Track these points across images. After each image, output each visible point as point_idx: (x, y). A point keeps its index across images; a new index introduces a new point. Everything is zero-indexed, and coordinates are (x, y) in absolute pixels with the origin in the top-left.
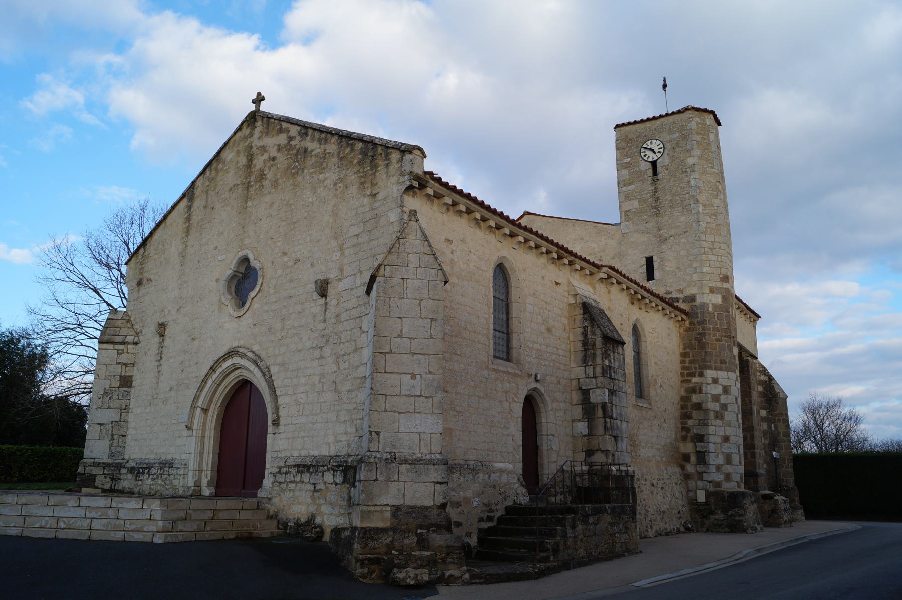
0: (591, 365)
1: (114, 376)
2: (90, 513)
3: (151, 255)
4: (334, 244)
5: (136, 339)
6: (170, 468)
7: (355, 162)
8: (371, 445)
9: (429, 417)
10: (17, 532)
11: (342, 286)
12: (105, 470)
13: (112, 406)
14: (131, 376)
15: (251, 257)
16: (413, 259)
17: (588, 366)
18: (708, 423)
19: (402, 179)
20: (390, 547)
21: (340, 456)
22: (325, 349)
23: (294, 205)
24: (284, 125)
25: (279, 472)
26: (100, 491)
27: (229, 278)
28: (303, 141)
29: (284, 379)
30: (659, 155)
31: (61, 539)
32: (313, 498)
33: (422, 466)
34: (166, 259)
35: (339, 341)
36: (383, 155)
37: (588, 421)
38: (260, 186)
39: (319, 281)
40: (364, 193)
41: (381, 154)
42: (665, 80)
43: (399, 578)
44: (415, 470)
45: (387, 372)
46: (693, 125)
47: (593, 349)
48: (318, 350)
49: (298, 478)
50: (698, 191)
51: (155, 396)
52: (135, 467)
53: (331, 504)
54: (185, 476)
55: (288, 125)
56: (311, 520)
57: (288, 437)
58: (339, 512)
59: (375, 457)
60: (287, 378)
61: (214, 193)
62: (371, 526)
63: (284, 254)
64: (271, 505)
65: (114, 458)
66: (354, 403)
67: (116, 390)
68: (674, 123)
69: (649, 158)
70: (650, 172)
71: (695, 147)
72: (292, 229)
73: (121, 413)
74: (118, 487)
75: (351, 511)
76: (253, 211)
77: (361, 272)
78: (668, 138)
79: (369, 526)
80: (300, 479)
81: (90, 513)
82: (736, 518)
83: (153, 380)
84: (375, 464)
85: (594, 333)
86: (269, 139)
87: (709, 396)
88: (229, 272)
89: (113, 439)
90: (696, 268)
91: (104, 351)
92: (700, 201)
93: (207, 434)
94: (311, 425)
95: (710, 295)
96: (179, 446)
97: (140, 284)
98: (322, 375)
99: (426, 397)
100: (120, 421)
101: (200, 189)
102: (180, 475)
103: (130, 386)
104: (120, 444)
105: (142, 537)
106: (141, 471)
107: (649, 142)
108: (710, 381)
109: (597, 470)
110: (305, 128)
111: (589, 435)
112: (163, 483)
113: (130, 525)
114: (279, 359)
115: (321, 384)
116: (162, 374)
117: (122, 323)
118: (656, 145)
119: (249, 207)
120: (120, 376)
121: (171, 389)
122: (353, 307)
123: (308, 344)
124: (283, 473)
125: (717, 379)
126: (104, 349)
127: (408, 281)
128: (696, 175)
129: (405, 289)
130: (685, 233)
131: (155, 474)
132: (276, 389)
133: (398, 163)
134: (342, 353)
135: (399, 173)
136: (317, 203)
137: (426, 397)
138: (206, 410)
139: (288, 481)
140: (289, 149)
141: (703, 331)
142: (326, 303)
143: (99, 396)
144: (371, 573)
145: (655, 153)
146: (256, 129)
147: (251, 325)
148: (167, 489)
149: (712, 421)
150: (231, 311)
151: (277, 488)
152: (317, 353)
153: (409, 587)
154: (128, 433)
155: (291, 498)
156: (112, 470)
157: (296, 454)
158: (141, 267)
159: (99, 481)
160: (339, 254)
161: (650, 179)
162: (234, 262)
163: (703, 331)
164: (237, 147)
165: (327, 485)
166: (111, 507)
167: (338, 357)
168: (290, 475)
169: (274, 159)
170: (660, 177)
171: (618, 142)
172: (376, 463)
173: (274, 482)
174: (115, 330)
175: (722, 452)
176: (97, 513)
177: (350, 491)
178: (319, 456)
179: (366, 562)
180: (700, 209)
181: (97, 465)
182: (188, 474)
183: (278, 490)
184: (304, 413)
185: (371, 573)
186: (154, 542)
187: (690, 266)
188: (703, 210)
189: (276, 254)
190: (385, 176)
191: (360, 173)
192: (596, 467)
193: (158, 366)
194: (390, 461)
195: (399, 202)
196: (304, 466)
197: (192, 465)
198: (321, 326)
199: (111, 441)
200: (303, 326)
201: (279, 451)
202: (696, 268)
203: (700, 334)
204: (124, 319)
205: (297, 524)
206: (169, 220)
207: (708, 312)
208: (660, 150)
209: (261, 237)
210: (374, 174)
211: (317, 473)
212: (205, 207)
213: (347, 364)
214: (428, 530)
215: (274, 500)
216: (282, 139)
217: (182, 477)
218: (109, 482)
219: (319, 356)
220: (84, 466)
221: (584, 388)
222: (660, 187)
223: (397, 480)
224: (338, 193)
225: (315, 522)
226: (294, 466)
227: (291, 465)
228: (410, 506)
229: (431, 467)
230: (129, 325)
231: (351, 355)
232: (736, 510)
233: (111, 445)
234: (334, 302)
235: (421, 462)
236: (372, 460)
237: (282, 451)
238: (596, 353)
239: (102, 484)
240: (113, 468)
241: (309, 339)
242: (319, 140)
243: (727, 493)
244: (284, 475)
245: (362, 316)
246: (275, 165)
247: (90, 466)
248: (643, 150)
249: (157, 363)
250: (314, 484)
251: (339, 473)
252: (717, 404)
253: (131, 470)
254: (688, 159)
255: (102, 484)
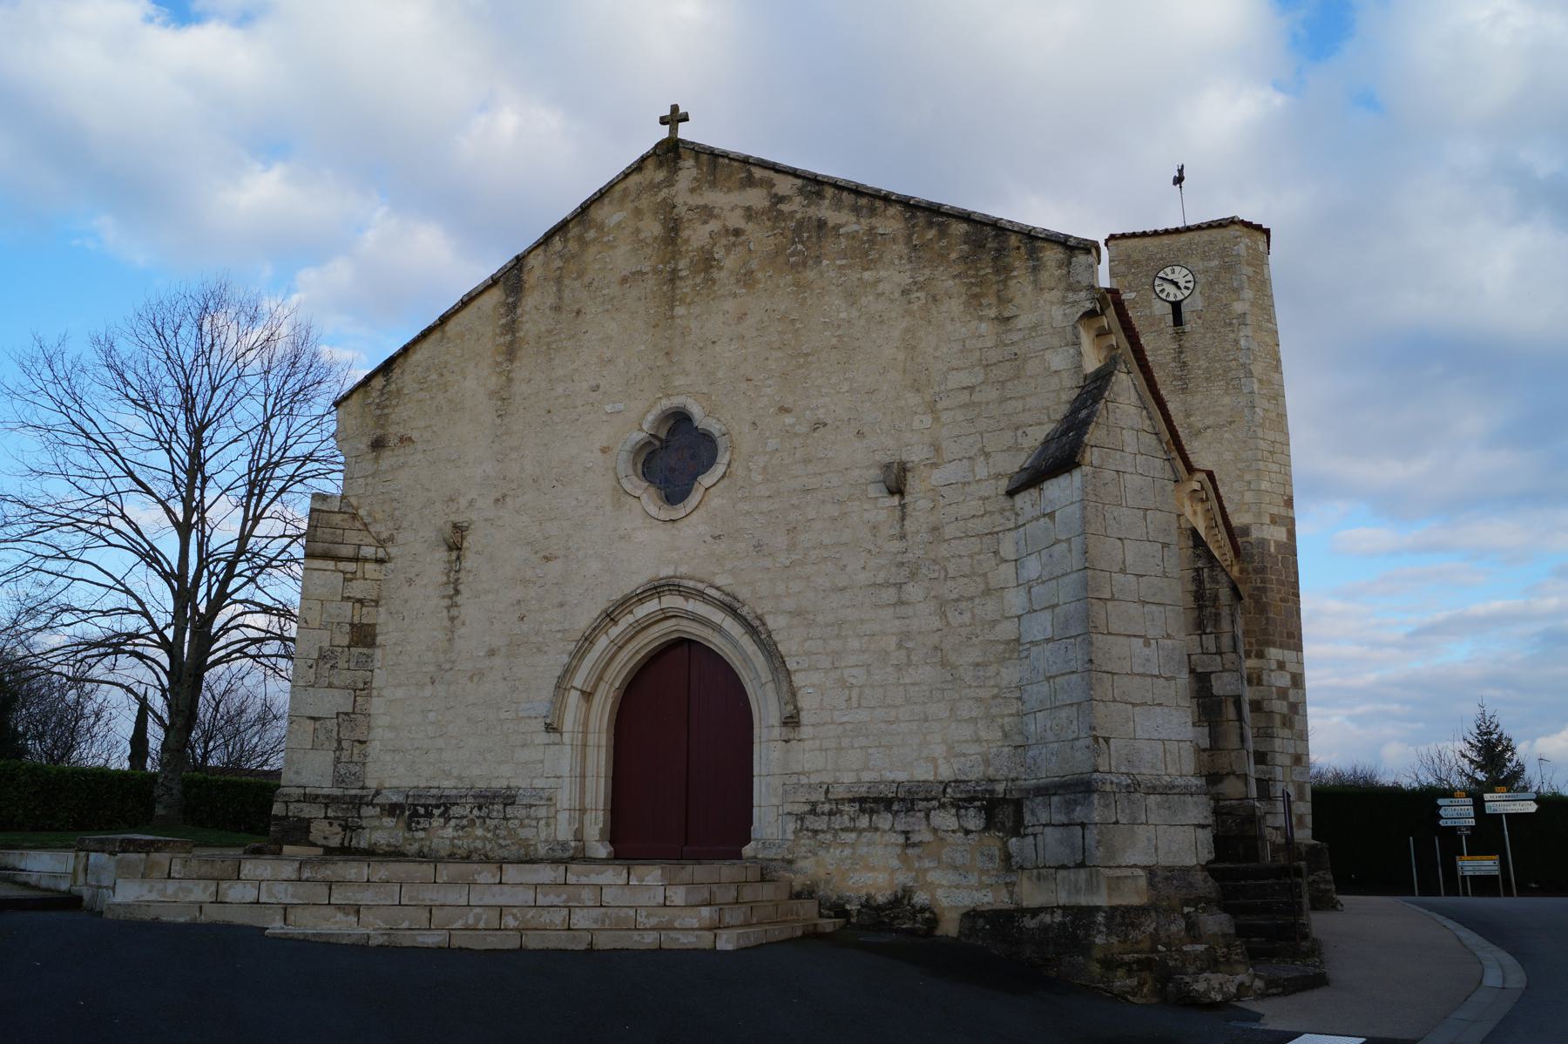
0: (1211, 633)
1: (338, 623)
2: (545, 896)
3: (406, 391)
4: (912, 399)
5: (381, 553)
6: (505, 805)
7: (953, 256)
8: (1100, 760)
9: (1174, 712)
10: (440, 938)
11: (938, 476)
12: (329, 811)
13: (336, 683)
14: (373, 626)
15: (696, 411)
16: (1128, 436)
17: (1206, 634)
18: (1273, 733)
19: (1071, 296)
20: (1155, 938)
21: (968, 781)
22: (909, 588)
23: (802, 323)
24: (758, 173)
25: (813, 812)
26: (320, 851)
27: (638, 446)
28: (813, 207)
29: (806, 640)
30: (1187, 293)
31: (535, 950)
32: (904, 859)
33: (1176, 797)
34: (449, 400)
35: (943, 574)
36: (1023, 250)
37: (1209, 725)
38: (706, 281)
39: (896, 465)
40: (980, 313)
41: (1018, 248)
42: (1181, 171)
43: (1197, 991)
44: (1167, 804)
45: (1110, 634)
46: (1241, 248)
47: (1214, 606)
48: (892, 591)
49: (864, 821)
50: (1252, 358)
51: (448, 666)
52: (401, 804)
53: (956, 868)
54: (550, 820)
55: (771, 174)
56: (903, 897)
57: (824, 747)
58: (980, 882)
59: (1112, 783)
60: (812, 639)
61: (577, 284)
62: (1124, 903)
63: (784, 410)
64: (795, 872)
65: (343, 785)
66: (994, 686)
67: (343, 652)
68: (1211, 242)
69: (1168, 295)
70: (1170, 319)
71: (1246, 285)
72: (800, 367)
73: (355, 697)
74: (359, 843)
75: (1014, 878)
76: (692, 326)
77: (987, 455)
78: (1201, 266)
79: (1119, 902)
80: (868, 824)
81: (545, 896)
82: (1322, 886)
83: (435, 633)
84: (1112, 795)
85: (1214, 580)
86: (722, 194)
87: (1274, 689)
88: (639, 437)
89: (340, 748)
90: (1249, 483)
91: (316, 573)
92: (1256, 374)
93: (592, 739)
94: (883, 726)
95: (1272, 527)
96: (526, 763)
97: (378, 445)
98: (904, 637)
99: (1166, 679)
100: (354, 713)
101: (538, 272)
102: (538, 820)
103: (371, 644)
104: (355, 758)
105: (695, 940)
106: (422, 811)
107: (1168, 270)
108: (1274, 666)
109: (1231, 806)
110: (814, 185)
111: (1211, 749)
112: (489, 835)
113: (647, 917)
114: (789, 604)
115: (904, 652)
116: (463, 624)
117: (343, 520)
118: (1180, 275)
119: (681, 317)
120: (350, 624)
121: (492, 653)
122: (974, 516)
123: (863, 577)
124: (823, 814)
125: (1284, 662)
126: (315, 569)
127: (1127, 476)
128: (1248, 331)
129: (1122, 489)
130: (1231, 423)
131: (462, 817)
132: (786, 659)
133: (1060, 267)
134: (954, 596)
135: (1064, 284)
136: (863, 322)
137: (1166, 679)
138: (590, 694)
139: (837, 827)
140: (776, 217)
141: (1262, 585)
142: (903, 506)
143: (310, 662)
144: (1141, 985)
145: (1179, 288)
146: (680, 173)
147: (708, 538)
148: (501, 846)
149: (1280, 732)
150: (653, 510)
151: (807, 842)
152: (889, 595)
153: (1213, 1006)
154: (372, 736)
155: (847, 858)
156: (343, 809)
157: (848, 778)
158: (378, 412)
159: (319, 830)
160: (931, 420)
161: (1170, 330)
162: (650, 417)
163: (1262, 585)
164: (633, 201)
165: (941, 834)
166: (566, 884)
167: (942, 606)
168: (842, 816)
169: (737, 232)
170: (1187, 328)
171: (1113, 264)
172: (1114, 793)
173: (801, 830)
174: (334, 533)
175: (1293, 781)
176: (559, 896)
177: (1005, 844)
178: (908, 782)
179: (1135, 967)
180: (1256, 386)
181: (313, 799)
182: (555, 817)
183: (810, 845)
184: (864, 703)
185: (1141, 985)
186: (718, 948)
187: (1240, 478)
188: (1259, 389)
189: (761, 408)
190: (1030, 288)
191: (967, 277)
192: (1228, 802)
193: (448, 608)
194: (1133, 790)
195: (1070, 337)
196: (876, 800)
197: (565, 798)
198: (896, 546)
199: (338, 753)
200: (846, 544)
201: (803, 773)
202: (1249, 483)
203: (1258, 589)
204: (345, 513)
205: (868, 905)
206: (452, 326)
207: (1270, 555)
208: (1188, 285)
209: (720, 374)
210: (1005, 282)
211: (911, 813)
212: (557, 309)
213: (967, 618)
214: (1196, 906)
215: (800, 864)
216: (756, 198)
217: (542, 822)
218: (338, 833)
219: (895, 600)
220: (286, 802)
221: (1199, 670)
222: (1187, 345)
223: (1144, 821)
224: (915, 308)
225: (913, 902)
226: (852, 800)
227: (843, 799)
228: (1166, 867)
229: (1189, 799)
230: (358, 524)
231: (977, 601)
232: (1321, 873)
233: (337, 760)
234: (924, 504)
235: (1173, 792)
236: (1108, 788)
237: (809, 773)
238: (1219, 614)
239: (325, 838)
240: (344, 806)
241: (864, 568)
242: (856, 210)
243: (1306, 845)
244: (826, 818)
245: (997, 533)
246: (741, 244)
247: (299, 801)
248: (1157, 282)
249: (447, 602)
250: (906, 833)
251: (972, 812)
252: (1285, 703)
253: (393, 810)
254: (1235, 303)
255: (325, 838)
